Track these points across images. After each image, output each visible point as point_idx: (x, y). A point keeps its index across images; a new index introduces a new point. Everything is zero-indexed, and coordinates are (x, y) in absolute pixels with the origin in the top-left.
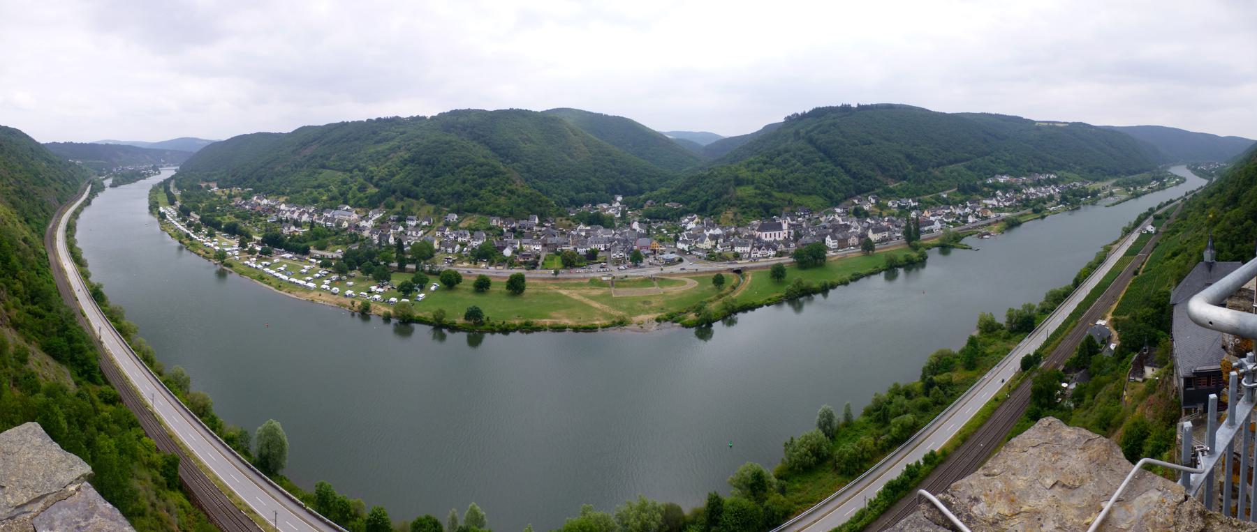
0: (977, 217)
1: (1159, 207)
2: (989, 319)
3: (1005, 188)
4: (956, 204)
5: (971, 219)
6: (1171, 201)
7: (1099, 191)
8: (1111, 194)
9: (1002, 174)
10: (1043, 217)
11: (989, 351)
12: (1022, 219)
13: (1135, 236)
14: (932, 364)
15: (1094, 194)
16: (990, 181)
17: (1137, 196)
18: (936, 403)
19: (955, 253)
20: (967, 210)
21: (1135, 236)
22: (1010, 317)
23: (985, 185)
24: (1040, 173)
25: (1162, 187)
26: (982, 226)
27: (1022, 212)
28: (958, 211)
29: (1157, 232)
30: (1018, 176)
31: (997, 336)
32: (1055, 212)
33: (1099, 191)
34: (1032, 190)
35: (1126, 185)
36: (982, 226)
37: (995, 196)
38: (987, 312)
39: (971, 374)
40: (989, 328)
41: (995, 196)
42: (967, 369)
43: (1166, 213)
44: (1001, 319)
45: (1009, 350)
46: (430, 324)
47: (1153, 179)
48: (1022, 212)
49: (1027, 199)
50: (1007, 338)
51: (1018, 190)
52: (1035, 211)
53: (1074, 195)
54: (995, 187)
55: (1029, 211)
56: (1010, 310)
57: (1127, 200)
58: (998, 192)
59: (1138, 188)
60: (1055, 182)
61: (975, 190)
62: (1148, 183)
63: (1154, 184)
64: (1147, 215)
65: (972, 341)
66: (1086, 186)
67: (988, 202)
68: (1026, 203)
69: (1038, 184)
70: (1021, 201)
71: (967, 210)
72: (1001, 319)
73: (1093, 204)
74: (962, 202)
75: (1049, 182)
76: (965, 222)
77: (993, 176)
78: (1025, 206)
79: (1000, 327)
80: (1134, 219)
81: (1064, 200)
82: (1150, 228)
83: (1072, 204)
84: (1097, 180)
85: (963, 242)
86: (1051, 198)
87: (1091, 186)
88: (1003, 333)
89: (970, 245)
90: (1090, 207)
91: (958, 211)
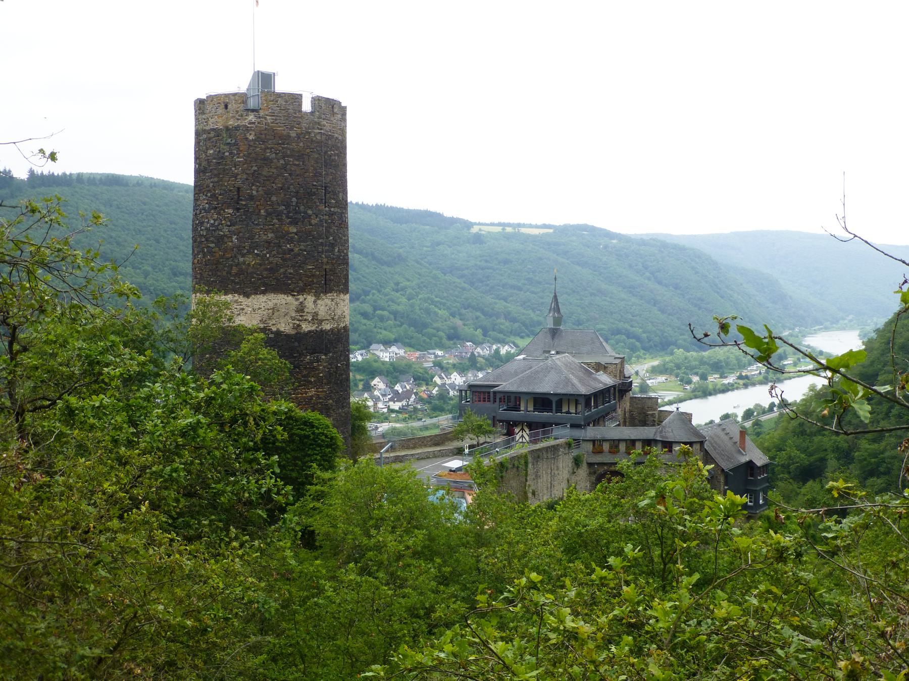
9: (387, 343)
49: (443, 396)
70: (430, 400)
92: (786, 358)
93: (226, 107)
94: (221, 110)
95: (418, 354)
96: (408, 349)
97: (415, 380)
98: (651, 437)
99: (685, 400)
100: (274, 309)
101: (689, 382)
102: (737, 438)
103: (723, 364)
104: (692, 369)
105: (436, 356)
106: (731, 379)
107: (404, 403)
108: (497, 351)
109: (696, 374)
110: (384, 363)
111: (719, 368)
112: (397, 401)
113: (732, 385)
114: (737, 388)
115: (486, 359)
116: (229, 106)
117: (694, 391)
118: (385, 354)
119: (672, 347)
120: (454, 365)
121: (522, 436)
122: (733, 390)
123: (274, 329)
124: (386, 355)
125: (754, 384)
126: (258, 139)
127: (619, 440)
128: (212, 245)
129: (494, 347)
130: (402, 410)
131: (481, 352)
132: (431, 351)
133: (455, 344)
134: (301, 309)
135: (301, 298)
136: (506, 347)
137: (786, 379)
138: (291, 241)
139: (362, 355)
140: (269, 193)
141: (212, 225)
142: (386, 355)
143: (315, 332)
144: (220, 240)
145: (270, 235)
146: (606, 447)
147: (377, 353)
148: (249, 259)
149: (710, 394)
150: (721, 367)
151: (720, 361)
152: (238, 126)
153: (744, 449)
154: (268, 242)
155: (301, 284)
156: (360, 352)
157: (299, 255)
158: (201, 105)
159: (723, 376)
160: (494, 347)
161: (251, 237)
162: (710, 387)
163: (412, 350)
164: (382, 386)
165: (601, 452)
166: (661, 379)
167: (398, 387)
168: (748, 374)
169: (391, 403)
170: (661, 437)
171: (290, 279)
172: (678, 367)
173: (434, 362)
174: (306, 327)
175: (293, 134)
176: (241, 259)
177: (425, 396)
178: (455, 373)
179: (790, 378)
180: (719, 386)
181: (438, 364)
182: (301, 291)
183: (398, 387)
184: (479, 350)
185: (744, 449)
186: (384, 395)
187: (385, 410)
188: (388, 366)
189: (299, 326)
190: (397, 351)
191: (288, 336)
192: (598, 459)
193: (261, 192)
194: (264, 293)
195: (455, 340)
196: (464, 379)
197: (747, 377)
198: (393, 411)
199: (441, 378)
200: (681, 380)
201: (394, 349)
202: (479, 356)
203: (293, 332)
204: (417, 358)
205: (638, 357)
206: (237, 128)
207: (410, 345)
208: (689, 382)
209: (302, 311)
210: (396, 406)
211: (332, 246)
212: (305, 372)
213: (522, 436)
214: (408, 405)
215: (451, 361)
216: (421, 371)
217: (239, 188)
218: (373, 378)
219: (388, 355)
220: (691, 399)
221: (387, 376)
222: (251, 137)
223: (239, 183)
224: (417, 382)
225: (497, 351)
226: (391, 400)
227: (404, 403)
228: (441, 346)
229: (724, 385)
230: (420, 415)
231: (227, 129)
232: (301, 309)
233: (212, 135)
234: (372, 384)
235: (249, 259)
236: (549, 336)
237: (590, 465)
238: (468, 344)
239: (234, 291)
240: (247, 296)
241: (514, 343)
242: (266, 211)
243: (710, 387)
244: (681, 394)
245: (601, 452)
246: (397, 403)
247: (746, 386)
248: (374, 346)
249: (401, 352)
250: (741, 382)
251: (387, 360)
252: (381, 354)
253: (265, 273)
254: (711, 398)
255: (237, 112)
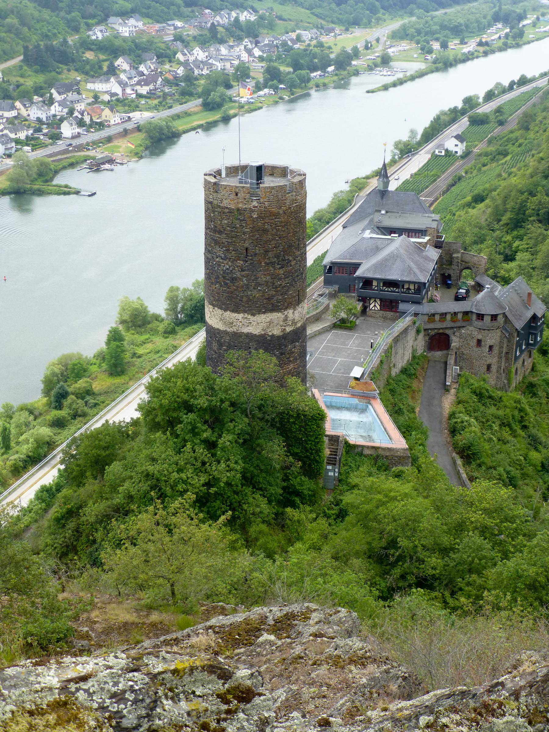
0: (81, 123)
1: (490, 96)
2: (136, 305)
3: (137, 50)
4: (26, 96)
5: (67, 130)
6: (523, 81)
7: (356, 54)
8: (385, 61)
9: (125, 14)
10: (226, 120)
11: (140, 351)
12: (179, 125)
13: (421, 159)
14: (54, 374)
15: (344, 62)
16: (98, 34)
17: (445, 64)
18: (75, 416)
19: (42, 206)
20: (55, 109)
21: (421, 159)
22: (173, 300)
23: (87, 45)
24: (216, 10)
25: (516, 40)
26: (95, 144)
27: (177, 109)
28: (35, 113)
29: (466, 154)
30: (161, 18)
31: (155, 332)
32: (252, 108)
33: (356, 54)
34: (199, 54)
35: (420, 37)
36: (95, 144)
37: (113, 71)
38: (133, 298)
39: (118, 380)
40: (138, 320)
41: (113, 71)
42: (111, 374)
43: (499, 110)
44: (158, 307)
45: (175, 348)
46: (9, 193)
47: (496, 18)
48: (177, 109)
49: (189, 79)
50: (170, 332)
51: (164, 56)
52: (209, 106)
53: (297, 66)
54: (112, 49)
55: (194, 104)
56: (172, 290)
57: (421, 75)
58: (121, 63)
59: (454, 44)
60: (251, 32)
61: (65, 58)
62: (481, 29)
63: (497, 32)
64: (454, 115)
65: (115, 337)
66: (327, 40)
67: (98, 86)
68: (186, 86)
69: (211, 37)
70: (174, 82)
71: (55, 109)
72: (158, 307)
73: (339, 86)
74: (38, 90)
75: (239, 32)
76: (56, 137)
77: (103, 20)
78: (187, 94)
79: (156, 318)
80: (422, 124)
81: (273, 77)
82: (452, 145)
83: (291, 87)
84: (356, 23)
85: (60, 180)
86: (243, 73)
87: (341, 41)
88: (161, 327)
89: (74, 184)
90: (332, 92)
91: (35, 113)
92: (526, 18)
93: (237, 195)
94: (233, 196)
95: (158, 26)
96: (146, 20)
97: (158, 57)
98: (468, 309)
99: (426, 74)
100: (270, 322)
101: (430, 52)
102: (525, 297)
103: (463, 27)
104: (431, 34)
105: (176, 28)
106: (471, 46)
107: (151, 87)
108: (237, 20)
109: (437, 39)
110: (125, 39)
111: (459, 31)
112: (145, 85)
113: (473, 54)
114: (477, 57)
115: (227, 29)
116: (239, 195)
117: (435, 62)
118: (124, 29)
119: (411, 6)
120: (195, 38)
121: (375, 306)
122: (473, 59)
123: (270, 334)
124: (127, 28)
125: (493, 52)
126: (259, 217)
127: (446, 313)
128: (228, 282)
129: (234, 14)
130: (150, 95)
131: (220, 20)
132: (170, 22)
133: (193, 11)
134: (286, 319)
135: (286, 312)
136: (245, 13)
137: (525, 44)
138: (280, 279)
139: (101, 31)
140: (267, 251)
141: (227, 269)
142: (127, 28)
143: (293, 331)
144: (233, 280)
145: (268, 277)
146: (437, 317)
147: (116, 27)
148: (255, 293)
149: (451, 65)
150: (462, 31)
151: (461, 25)
152: (246, 208)
153: (529, 305)
154: (267, 282)
155: (286, 304)
156: (99, 28)
157: (285, 287)
158: (213, 188)
159: (463, 42)
160: (234, 14)
161: (256, 279)
162: (451, 58)
163: (151, 21)
164: (126, 66)
165: (434, 321)
166: (404, 45)
167: (142, 68)
168: (488, 39)
169: (138, 87)
170: (477, 310)
171: (280, 302)
172: (419, 32)
173: (175, 36)
174: (288, 329)
175: (281, 212)
176: (249, 293)
177: (170, 77)
178: (197, 49)
179: (529, 43)
180: (459, 56)
181: (178, 38)
182: (286, 308)
183: (142, 68)
184: (218, 18)
185: (529, 305)
186: (130, 78)
187: (134, 96)
188: (130, 43)
189: (285, 329)
190: (136, 24)
191: (279, 337)
192: (431, 326)
193: (262, 251)
194: (264, 313)
195: (194, 8)
196: (206, 54)
197: (487, 44)
198: (140, 96)
199: (184, 54)
200: (422, 49)
201: (132, 21)
202: (219, 25)
203: (281, 334)
204: (157, 31)
205: (378, 19)
206: (245, 209)
207: (147, 16)
208: (430, 52)
209: (286, 320)
210: (144, 90)
211: (302, 273)
212: (288, 356)
213: (375, 306)
214: (156, 89)
215: (190, 33)
216: (163, 46)
217: (247, 249)
218: (116, 58)
219: (127, 29)
220: (432, 72)
221: (129, 55)
222: (255, 216)
223: (246, 245)
224: (160, 60)
225: (237, 20)
226: (139, 83)
227: (151, 87)
228: (180, 16)
229: (464, 54)
230: (169, 101)
231: (238, 210)
232: (286, 319)
233: (227, 211)
234: (116, 64)
235: (255, 293)
236: (379, 196)
237: (425, 330)
238: (207, 11)
239: (244, 312)
240: (253, 315)
241: (252, 8)
242: (265, 263)
243: (451, 58)
244: (422, 66)
245: (434, 321)
246: (144, 87)
247: (486, 54)
248: (112, 19)
249: (140, 24)
250: (481, 49)
251: (127, 34)
252: (120, 29)
253: (265, 301)
254: (451, 70)
255: (245, 199)
